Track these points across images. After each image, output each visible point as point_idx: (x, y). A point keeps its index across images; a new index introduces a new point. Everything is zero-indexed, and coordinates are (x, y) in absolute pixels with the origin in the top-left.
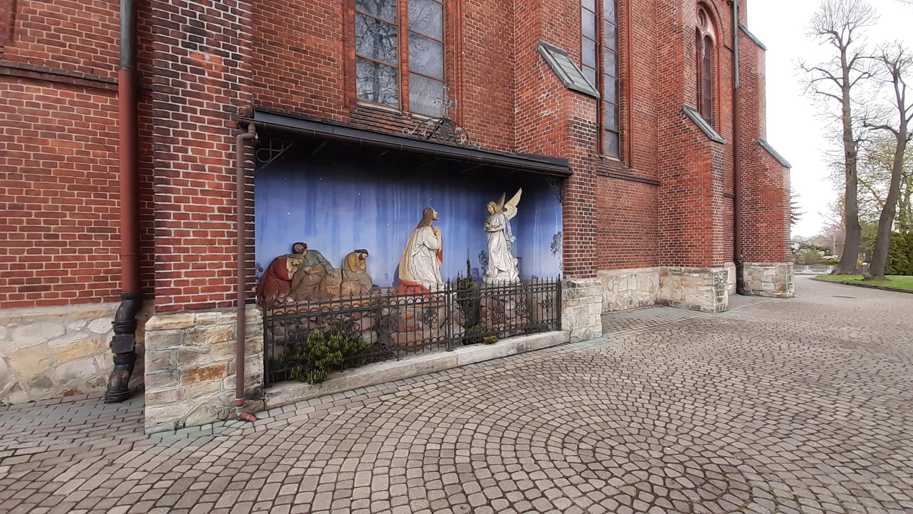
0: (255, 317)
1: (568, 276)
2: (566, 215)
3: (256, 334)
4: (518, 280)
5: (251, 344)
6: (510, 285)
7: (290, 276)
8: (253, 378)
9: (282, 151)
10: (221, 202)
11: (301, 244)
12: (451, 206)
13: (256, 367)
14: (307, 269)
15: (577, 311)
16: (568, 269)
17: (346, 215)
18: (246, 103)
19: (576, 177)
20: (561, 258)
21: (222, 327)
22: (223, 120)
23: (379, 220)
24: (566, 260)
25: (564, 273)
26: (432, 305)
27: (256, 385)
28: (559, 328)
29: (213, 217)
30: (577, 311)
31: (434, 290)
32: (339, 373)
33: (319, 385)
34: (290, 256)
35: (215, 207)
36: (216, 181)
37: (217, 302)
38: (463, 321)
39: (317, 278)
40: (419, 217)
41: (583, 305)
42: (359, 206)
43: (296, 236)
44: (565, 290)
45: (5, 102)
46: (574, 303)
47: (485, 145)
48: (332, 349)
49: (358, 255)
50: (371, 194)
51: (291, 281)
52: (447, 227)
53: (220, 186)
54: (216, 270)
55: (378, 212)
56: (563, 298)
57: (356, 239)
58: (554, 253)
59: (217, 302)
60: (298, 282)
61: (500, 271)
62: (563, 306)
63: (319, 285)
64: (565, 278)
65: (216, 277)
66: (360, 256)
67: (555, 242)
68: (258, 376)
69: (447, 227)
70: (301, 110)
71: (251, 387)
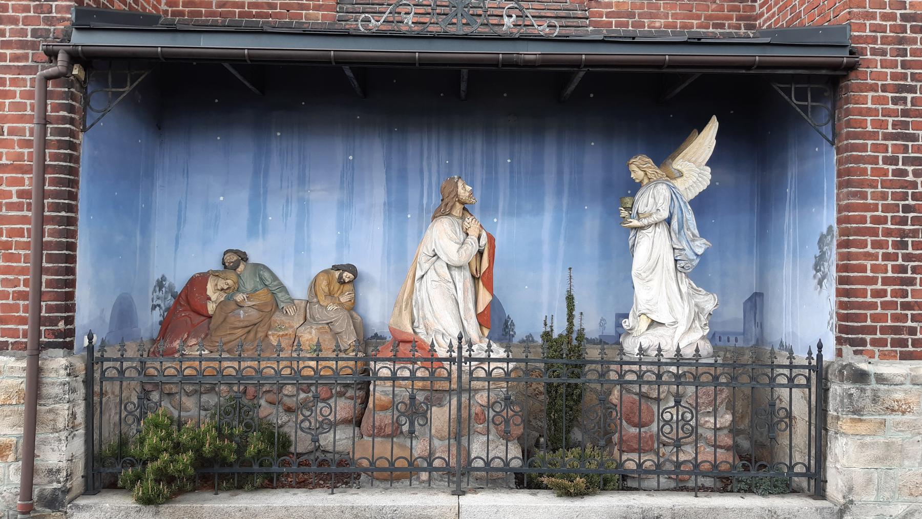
0: (57, 371)
1: (847, 350)
2: (845, 179)
3: (58, 399)
4: (706, 348)
5: (51, 416)
6: (678, 359)
7: (211, 308)
8: (50, 471)
9: (127, 89)
10: (21, 182)
11: (236, 252)
12: (560, 173)
13: (61, 453)
14: (239, 297)
15: (871, 453)
16: (850, 331)
17: (323, 199)
18: (64, 19)
19: (877, 68)
20: (833, 298)
21: (10, 381)
22: (30, 52)
23: (388, 205)
24: (842, 305)
25: (839, 341)
26: (438, 385)
27: (55, 485)
28: (820, 493)
29: (11, 207)
30: (871, 453)
31: (442, 352)
32: (208, 495)
33: (152, 508)
34: (216, 274)
35: (14, 189)
36: (17, 149)
37: (11, 340)
38: (518, 431)
39: (254, 315)
40: (436, 201)
41: (898, 438)
42: (350, 182)
43: (234, 237)
44: (836, 389)
45: (914, 77)
46: (861, 428)
47: (658, 23)
48: (178, 448)
49: (337, 274)
50: (373, 154)
51: (210, 317)
52: (548, 218)
53: (20, 156)
54: (11, 290)
55: (389, 192)
56: (832, 412)
57: (342, 244)
58: (820, 283)
59: (11, 340)
60: (222, 319)
61: (653, 324)
62: (831, 433)
63: (253, 326)
64: (839, 353)
65: (10, 301)
66: (341, 277)
67: (823, 254)
68: (59, 471)
69: (548, 218)
70: (249, 15)
71: (45, 485)
